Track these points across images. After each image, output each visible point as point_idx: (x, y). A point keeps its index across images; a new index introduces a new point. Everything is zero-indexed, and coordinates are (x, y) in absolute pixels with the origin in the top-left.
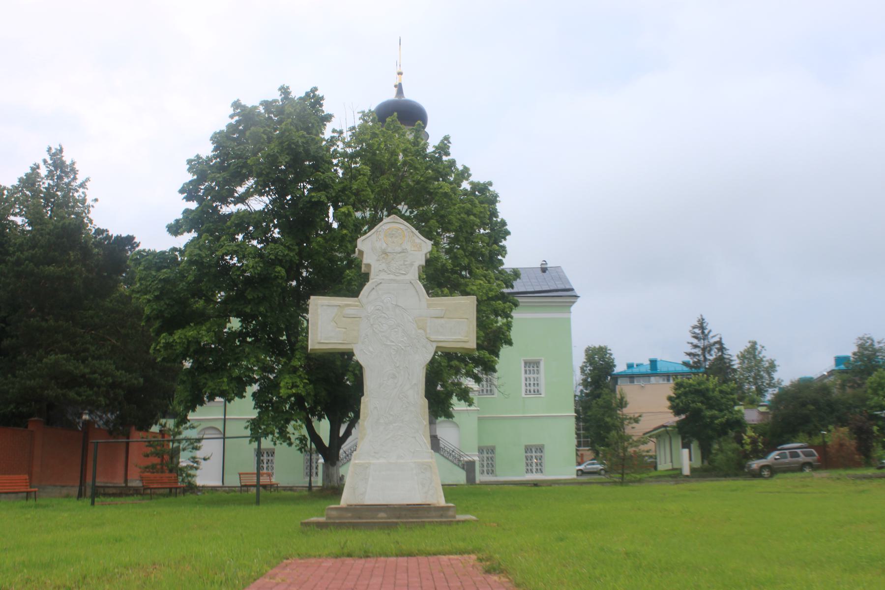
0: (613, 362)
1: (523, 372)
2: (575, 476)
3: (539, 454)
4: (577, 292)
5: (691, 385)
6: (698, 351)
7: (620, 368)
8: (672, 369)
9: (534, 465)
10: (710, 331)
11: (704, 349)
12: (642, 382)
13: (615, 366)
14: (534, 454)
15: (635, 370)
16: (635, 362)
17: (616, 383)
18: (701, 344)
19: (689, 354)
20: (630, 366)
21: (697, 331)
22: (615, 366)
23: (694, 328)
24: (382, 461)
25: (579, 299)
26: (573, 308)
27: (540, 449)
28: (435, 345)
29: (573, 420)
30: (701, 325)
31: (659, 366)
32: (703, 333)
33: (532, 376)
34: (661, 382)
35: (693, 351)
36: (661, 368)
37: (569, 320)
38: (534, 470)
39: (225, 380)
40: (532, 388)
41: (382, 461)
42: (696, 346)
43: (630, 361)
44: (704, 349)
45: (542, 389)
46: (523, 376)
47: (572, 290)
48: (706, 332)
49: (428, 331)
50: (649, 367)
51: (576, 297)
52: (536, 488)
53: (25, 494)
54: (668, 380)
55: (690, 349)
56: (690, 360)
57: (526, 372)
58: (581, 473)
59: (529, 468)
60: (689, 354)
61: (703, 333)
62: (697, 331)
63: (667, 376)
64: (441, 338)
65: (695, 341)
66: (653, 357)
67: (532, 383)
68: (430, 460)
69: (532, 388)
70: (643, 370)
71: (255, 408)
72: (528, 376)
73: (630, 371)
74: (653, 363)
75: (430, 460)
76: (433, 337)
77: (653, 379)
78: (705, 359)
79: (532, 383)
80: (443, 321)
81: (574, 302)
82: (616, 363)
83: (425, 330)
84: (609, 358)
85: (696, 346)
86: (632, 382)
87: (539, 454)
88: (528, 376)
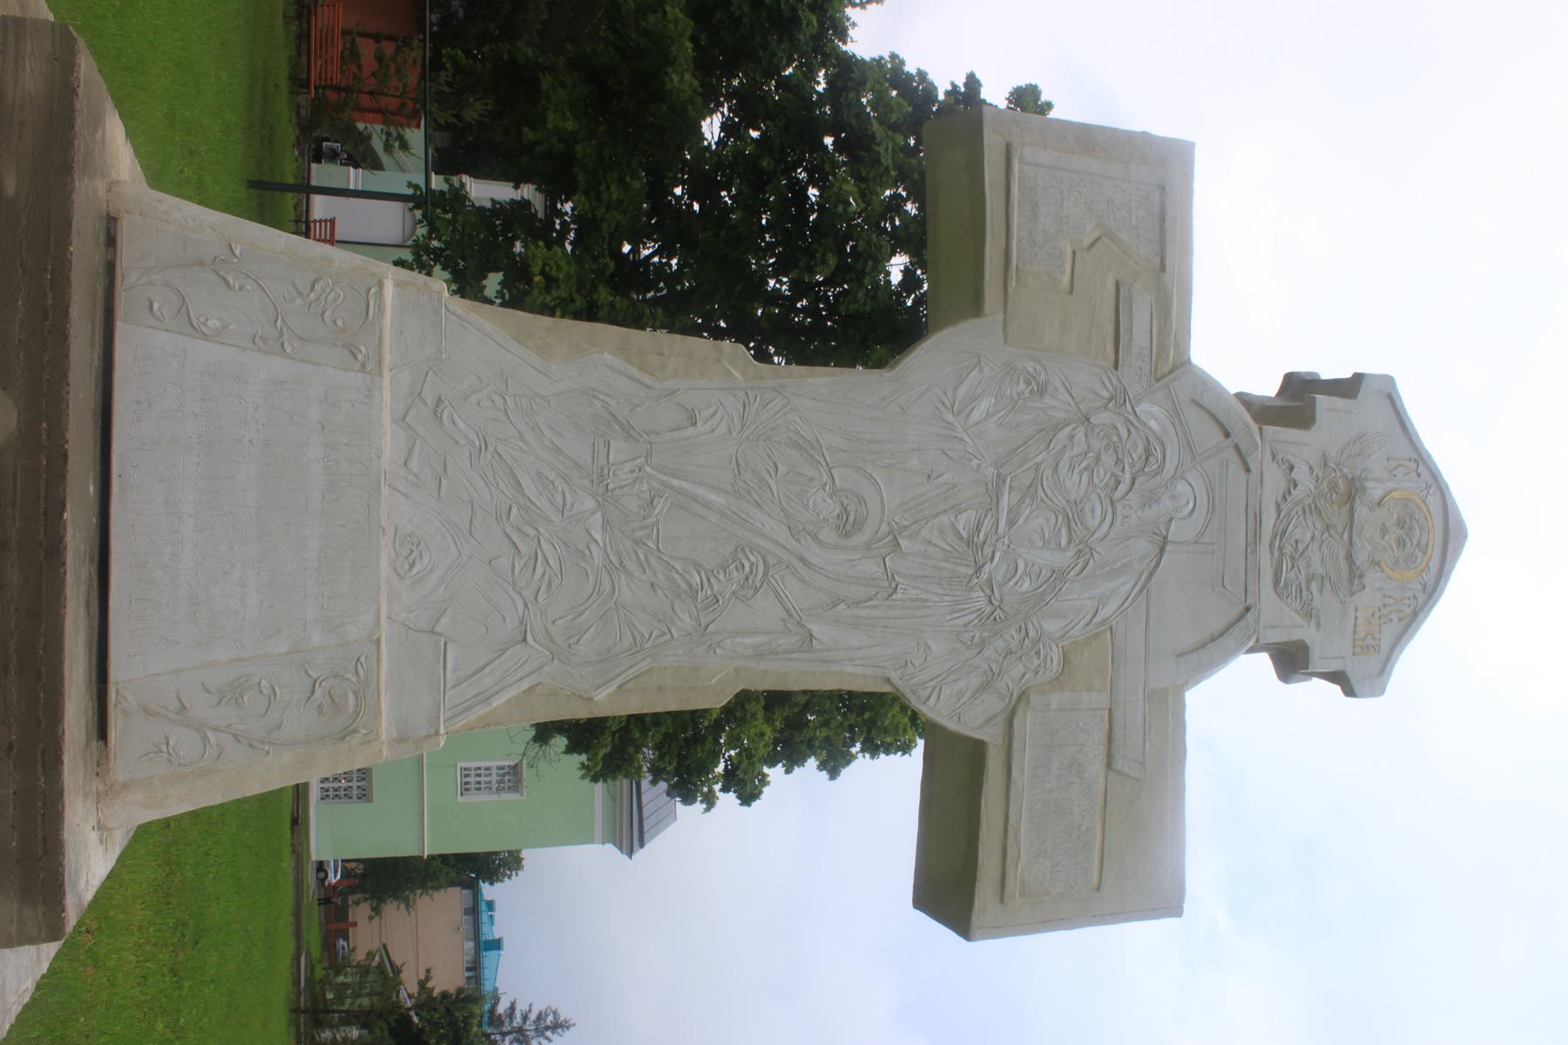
0: (498, 880)
1: (501, 763)
2: (314, 858)
3: (355, 792)
4: (640, 854)
5: (468, 1031)
6: (518, 1020)
7: (488, 891)
8: (487, 974)
9: (336, 785)
10: (547, 1038)
11: (520, 1030)
12: (466, 928)
13: (492, 884)
14: (355, 784)
15: (484, 917)
16: (497, 914)
17: (465, 887)
18: (530, 1025)
19: (512, 1008)
20: (490, 905)
21: (550, 1018)
22: (492, 884)
23: (555, 1013)
24: (389, 443)
25: (626, 857)
26: (610, 847)
27: (365, 795)
28: (991, 736)
29: (415, 853)
30: (559, 1026)
31: (492, 954)
32: (547, 1028)
33: (494, 778)
34: (466, 958)
35: (518, 1014)
36: (489, 957)
37: (592, 841)
38: (326, 785)
39: (570, 125)
40: (472, 779)
41: (389, 443)
42: (525, 1018)
43: (497, 906)
44: (520, 1030)
45: (472, 798)
46: (494, 764)
47: (642, 845)
48: (548, 1033)
49: (1055, 699)
50: (490, 938)
51: (630, 853)
52: (288, 824)
53: (304, 76)
54: (468, 969)
55: (521, 1007)
56: (502, 1008)
57: (502, 768)
58: (321, 867)
59: (331, 793)
60: (512, 1008)
61: (547, 1028)
62: (550, 1018)
63: (475, 967)
64: (1025, 760)
65: (533, 1016)
66: (505, 944)
67: (482, 779)
68: (386, 728)
69: (472, 779)
70: (485, 928)
71: (492, 200)
72: (494, 771)
73: (483, 907)
74: (496, 944)
75: (386, 728)
76: (1027, 723)
77: (471, 944)
78: (504, 1034)
79: (482, 779)
80: (1096, 769)
81: (621, 849)
82: (497, 885)
83: (1057, 683)
84: (504, 875)
85: (525, 1018)
86: (467, 912)
87: (355, 792)
88: (494, 771)
